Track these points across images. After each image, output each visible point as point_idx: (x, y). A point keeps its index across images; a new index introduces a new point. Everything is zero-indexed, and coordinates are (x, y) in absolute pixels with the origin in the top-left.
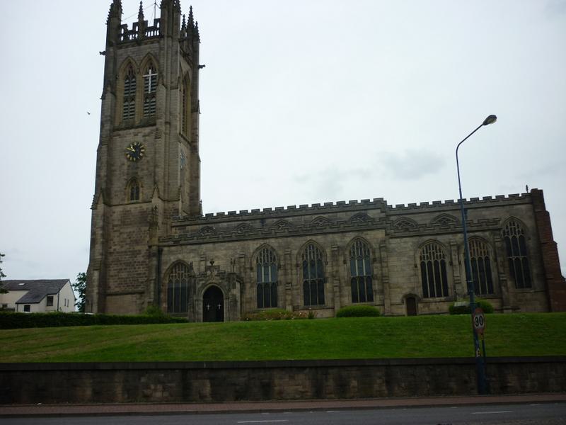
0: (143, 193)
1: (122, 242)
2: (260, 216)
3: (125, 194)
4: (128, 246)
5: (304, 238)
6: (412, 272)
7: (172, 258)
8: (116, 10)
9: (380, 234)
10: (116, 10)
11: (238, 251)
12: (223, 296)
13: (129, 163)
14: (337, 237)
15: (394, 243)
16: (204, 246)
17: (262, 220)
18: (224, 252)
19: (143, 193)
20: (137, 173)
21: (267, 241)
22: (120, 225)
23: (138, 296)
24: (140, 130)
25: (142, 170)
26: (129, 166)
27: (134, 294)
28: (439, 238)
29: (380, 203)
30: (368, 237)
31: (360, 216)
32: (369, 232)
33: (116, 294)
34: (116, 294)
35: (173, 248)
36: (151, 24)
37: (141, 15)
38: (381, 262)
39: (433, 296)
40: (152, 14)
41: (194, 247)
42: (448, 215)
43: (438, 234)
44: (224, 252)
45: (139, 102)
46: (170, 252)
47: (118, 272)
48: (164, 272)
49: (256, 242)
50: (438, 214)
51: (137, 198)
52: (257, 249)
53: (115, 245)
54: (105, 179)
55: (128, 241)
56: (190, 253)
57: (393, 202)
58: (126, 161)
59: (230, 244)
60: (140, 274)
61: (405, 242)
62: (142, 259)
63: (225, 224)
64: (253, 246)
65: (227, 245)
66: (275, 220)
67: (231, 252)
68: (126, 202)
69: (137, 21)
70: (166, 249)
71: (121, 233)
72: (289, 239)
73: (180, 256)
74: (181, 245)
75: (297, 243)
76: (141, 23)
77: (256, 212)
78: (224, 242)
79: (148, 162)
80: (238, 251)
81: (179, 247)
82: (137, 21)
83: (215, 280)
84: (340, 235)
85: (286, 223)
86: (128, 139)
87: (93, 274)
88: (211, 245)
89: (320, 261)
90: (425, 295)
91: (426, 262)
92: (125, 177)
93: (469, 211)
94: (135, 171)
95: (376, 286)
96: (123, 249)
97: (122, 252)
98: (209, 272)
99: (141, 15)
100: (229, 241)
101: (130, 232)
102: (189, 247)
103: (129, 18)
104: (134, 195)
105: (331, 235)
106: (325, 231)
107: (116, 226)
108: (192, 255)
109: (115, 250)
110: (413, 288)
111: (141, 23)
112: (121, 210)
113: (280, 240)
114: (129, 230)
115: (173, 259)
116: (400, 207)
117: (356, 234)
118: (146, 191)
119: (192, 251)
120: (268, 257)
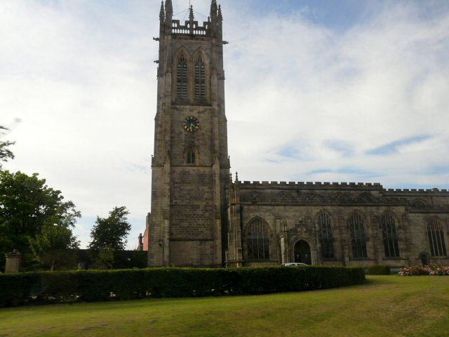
0: (199, 159)
1: (182, 197)
2: (296, 187)
3: (183, 158)
4: (188, 201)
5: (351, 207)
6: (424, 238)
7: (251, 215)
8: (167, 11)
9: (402, 209)
10: (167, 11)
11: (304, 214)
12: (309, 248)
13: (186, 133)
14: (374, 209)
15: (411, 216)
16: (277, 208)
17: (298, 191)
18: (293, 213)
19: (199, 159)
20: (193, 142)
21: (325, 207)
22: (180, 183)
23: (198, 243)
24: (194, 107)
25: (199, 140)
26: (186, 135)
27: (195, 240)
28: (439, 215)
29: (378, 187)
30: (394, 211)
31: (365, 194)
32: (395, 207)
33: (180, 240)
34: (180, 240)
35: (251, 207)
36: (200, 25)
37: (191, 15)
38: (405, 230)
39: (437, 255)
40: (202, 17)
41: (269, 207)
42: (421, 199)
43: (439, 213)
44: (293, 213)
45: (191, 86)
46: (253, 211)
47: (180, 222)
48: (245, 225)
49: (317, 207)
50: (414, 198)
51: (194, 161)
52: (318, 213)
53: (176, 199)
54: (169, 143)
55: (188, 197)
56: (266, 212)
57: (386, 186)
58: (183, 130)
59: (297, 208)
60: (200, 225)
61: (418, 216)
62: (201, 213)
63: (269, 191)
64: (315, 211)
65: (295, 208)
66: (277, 191)
67: (298, 214)
68: (185, 164)
69: (189, 20)
70: (246, 207)
71: (181, 190)
72: (341, 208)
73: (258, 214)
74: (259, 205)
75: (347, 211)
76: (191, 21)
77: (292, 184)
78: (293, 205)
79: (203, 134)
80: (304, 214)
81: (256, 207)
82: (189, 20)
83: (304, 236)
84: (376, 207)
85: (315, 195)
86: (187, 112)
87: (215, 222)
88: (282, 207)
89: (362, 225)
90: (433, 254)
91: (431, 231)
92: (183, 144)
93: (434, 198)
94: (193, 140)
95: (401, 246)
96: (184, 203)
97: (182, 206)
98: (299, 229)
99: (191, 15)
100: (296, 206)
101: (189, 190)
102: (265, 207)
103: (180, 15)
104: (191, 159)
105: (369, 207)
106: (365, 204)
107: (177, 183)
108: (268, 214)
109: (176, 203)
110: (425, 249)
111: (191, 21)
112: (181, 170)
113: (334, 208)
114: (188, 188)
115: (252, 215)
116: (391, 190)
117: (386, 208)
118: (202, 158)
119: (267, 210)
120: (354, 224)
